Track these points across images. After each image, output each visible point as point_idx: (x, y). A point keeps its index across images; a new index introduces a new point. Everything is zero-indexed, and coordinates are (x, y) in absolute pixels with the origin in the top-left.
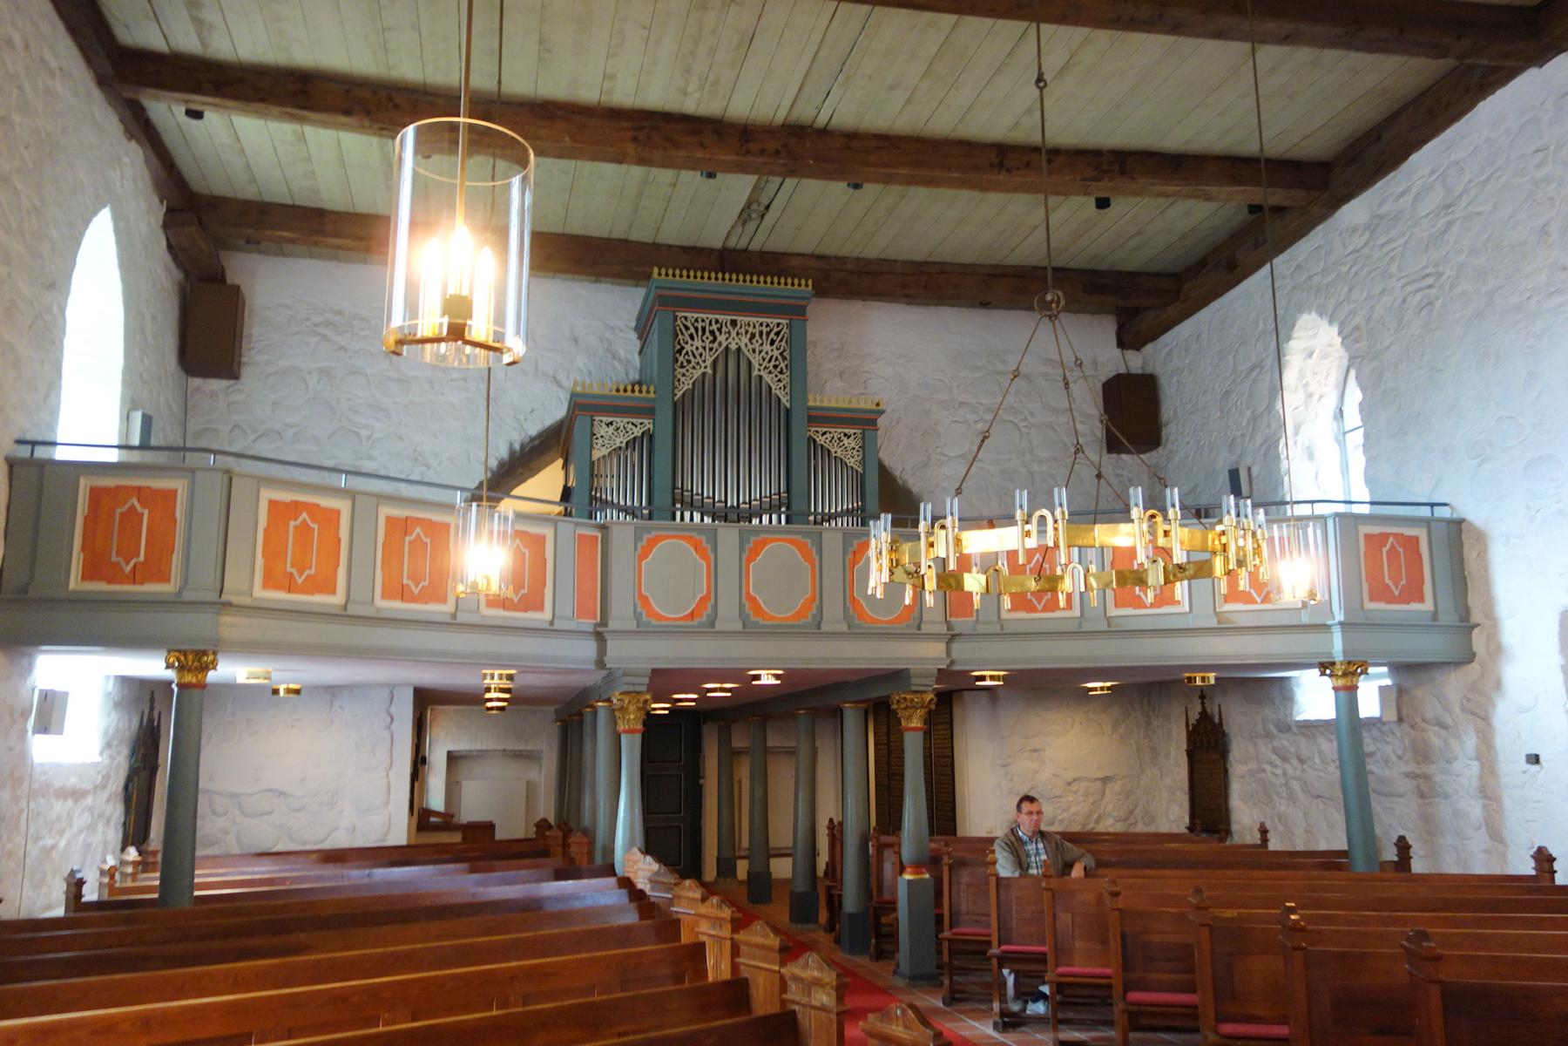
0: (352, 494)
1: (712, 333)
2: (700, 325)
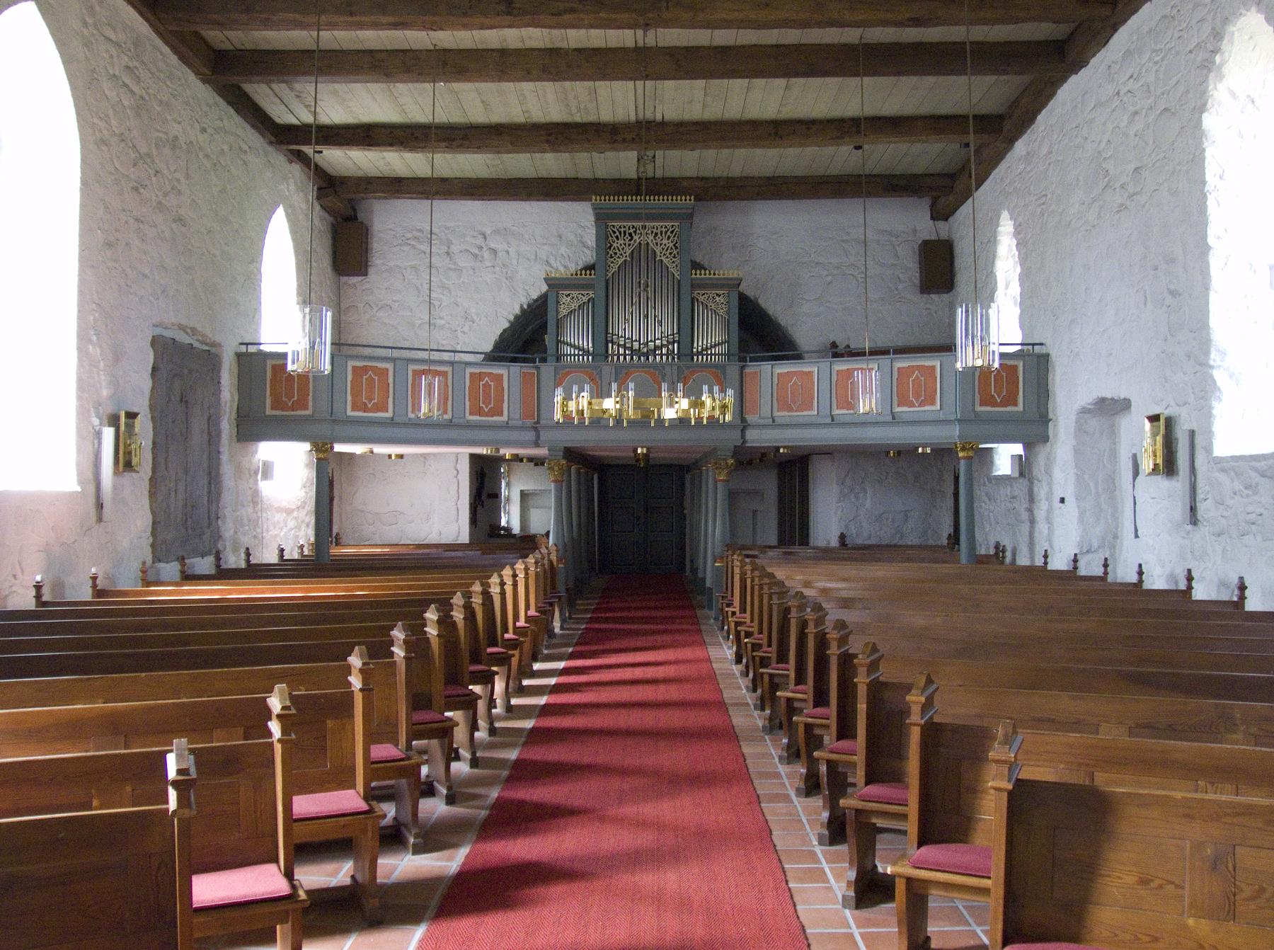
0: (394, 360)
1: (630, 235)
2: (622, 230)
